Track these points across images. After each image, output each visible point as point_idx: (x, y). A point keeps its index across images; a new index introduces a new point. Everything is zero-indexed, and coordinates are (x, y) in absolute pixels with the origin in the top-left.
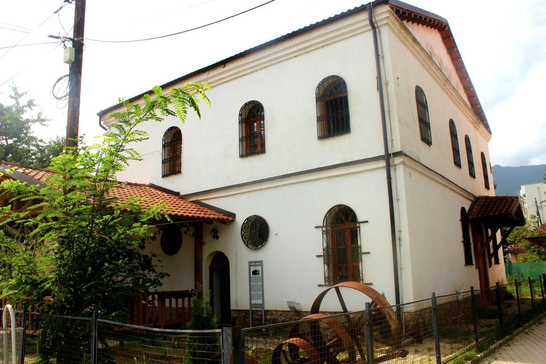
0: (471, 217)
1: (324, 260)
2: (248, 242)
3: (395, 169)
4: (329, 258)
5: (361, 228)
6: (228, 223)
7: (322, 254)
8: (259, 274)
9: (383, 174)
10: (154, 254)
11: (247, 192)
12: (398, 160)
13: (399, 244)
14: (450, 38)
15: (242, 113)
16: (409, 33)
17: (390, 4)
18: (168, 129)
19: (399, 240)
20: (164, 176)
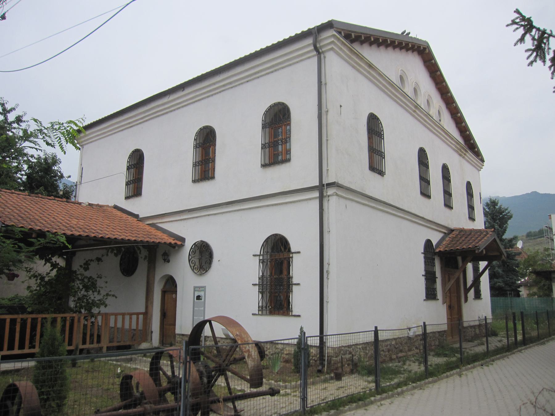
0: (437, 250)
1: (259, 289)
2: (194, 267)
3: (328, 200)
4: (264, 287)
5: (293, 259)
6: (177, 248)
7: (258, 283)
8: (201, 299)
9: (316, 204)
10: (100, 276)
11: (215, 214)
12: (330, 191)
13: (326, 276)
14: (432, 62)
15: (197, 138)
16: (362, 58)
17: (336, 28)
18: (133, 151)
19: (327, 272)
20: (127, 198)
